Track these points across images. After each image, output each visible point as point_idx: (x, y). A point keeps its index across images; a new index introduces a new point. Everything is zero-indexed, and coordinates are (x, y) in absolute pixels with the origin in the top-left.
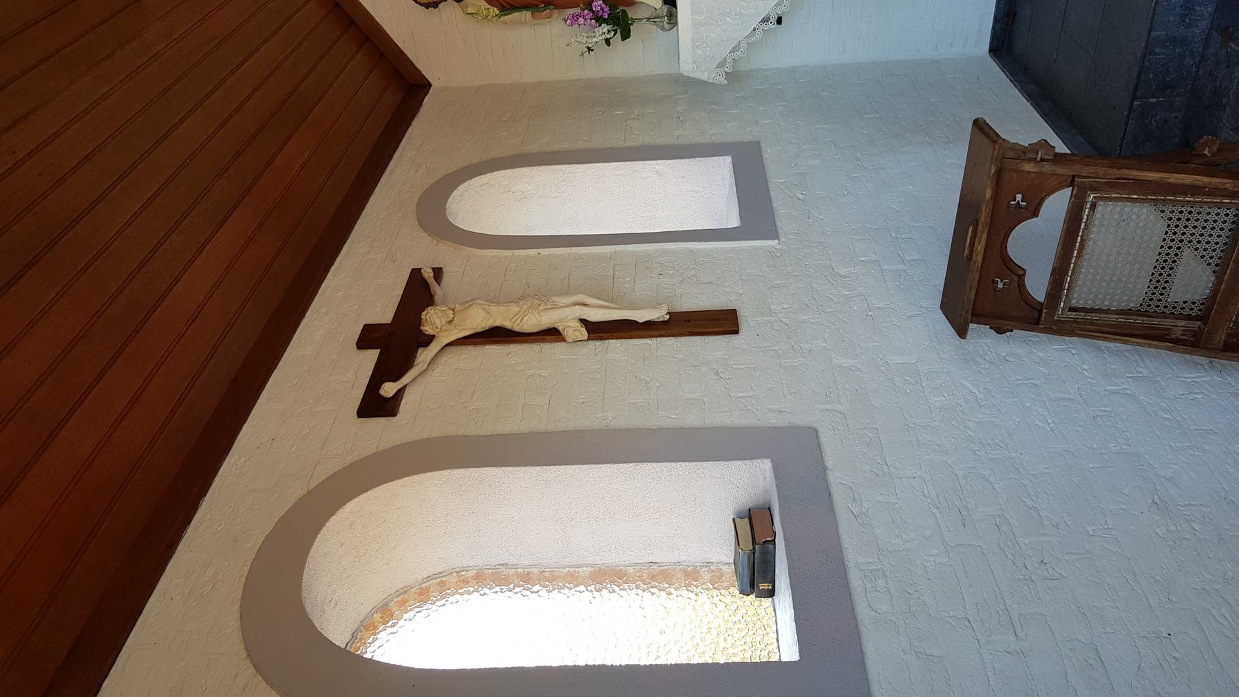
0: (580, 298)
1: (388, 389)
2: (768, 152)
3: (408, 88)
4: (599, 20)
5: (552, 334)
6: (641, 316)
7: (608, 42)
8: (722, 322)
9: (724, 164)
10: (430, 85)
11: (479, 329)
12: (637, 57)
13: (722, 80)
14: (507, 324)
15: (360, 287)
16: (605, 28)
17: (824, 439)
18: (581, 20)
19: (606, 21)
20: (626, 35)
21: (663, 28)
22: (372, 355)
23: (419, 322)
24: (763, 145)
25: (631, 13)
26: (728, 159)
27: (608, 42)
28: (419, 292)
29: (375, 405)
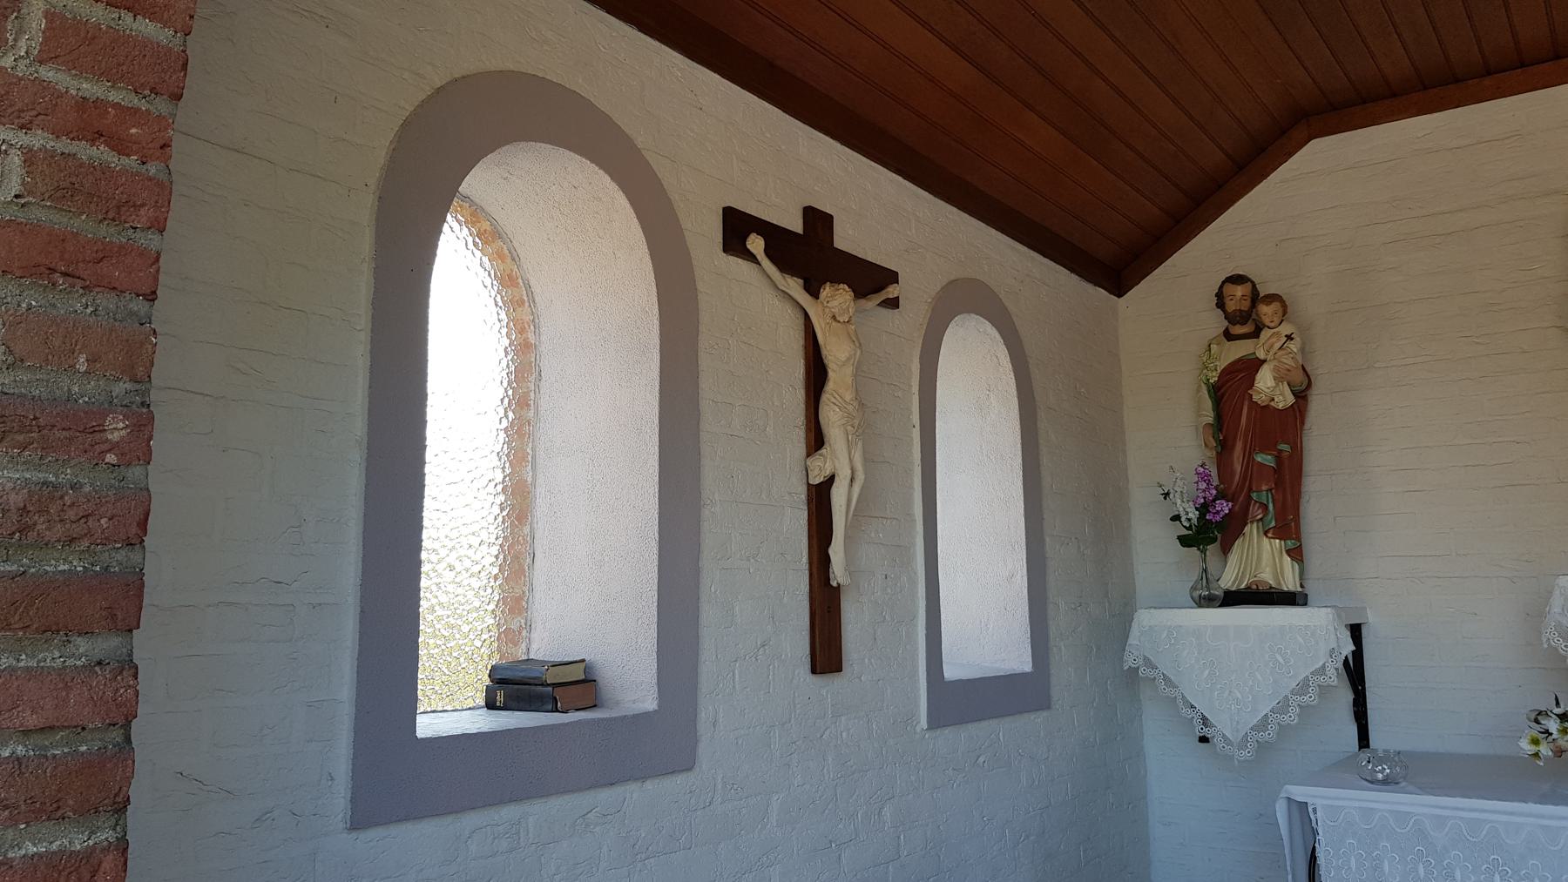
0: (860, 477)
1: (756, 244)
2: (1037, 719)
3: (1117, 270)
4: (1204, 509)
5: (816, 440)
6: (836, 552)
7: (1176, 518)
8: (826, 654)
9: (1020, 661)
10: (1119, 296)
11: (824, 352)
12: (1156, 552)
13: (1129, 662)
14: (830, 386)
15: (877, 208)
16: (1194, 515)
17: (679, 779)
18: (1203, 485)
19: (1202, 516)
20: (1185, 541)
21: (1193, 588)
22: (796, 226)
23: (836, 281)
24: (1045, 714)
25: (1212, 549)
26: (1028, 668)
27: (1176, 518)
28: (870, 280)
29: (737, 228)
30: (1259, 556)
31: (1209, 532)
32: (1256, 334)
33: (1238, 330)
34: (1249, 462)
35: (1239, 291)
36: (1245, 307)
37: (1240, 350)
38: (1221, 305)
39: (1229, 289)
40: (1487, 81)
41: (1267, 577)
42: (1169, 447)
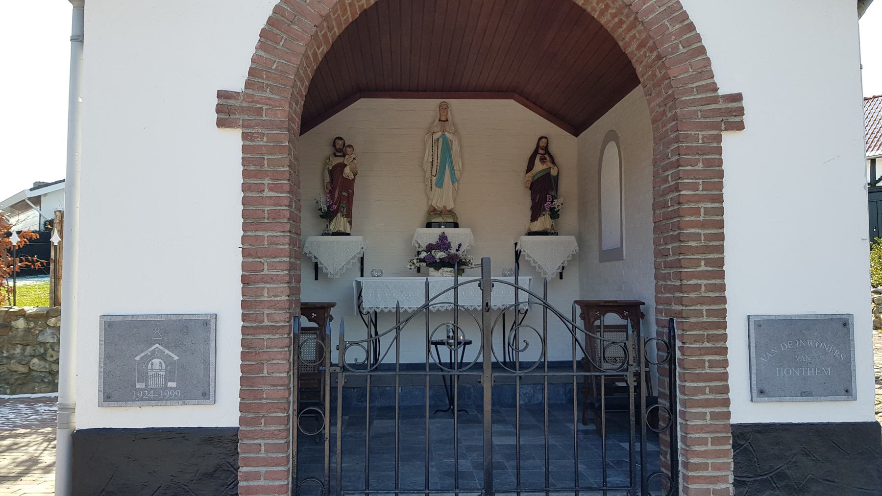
4: (329, 207)
12: (308, 221)
16: (326, 208)
20: (322, 217)
27: (320, 209)
30: (340, 223)
31: (328, 215)
32: (344, 156)
33: (339, 154)
34: (340, 195)
35: (341, 142)
36: (340, 148)
37: (339, 160)
38: (334, 145)
39: (337, 141)
40: (409, 93)
41: (342, 229)
42: (315, 190)
